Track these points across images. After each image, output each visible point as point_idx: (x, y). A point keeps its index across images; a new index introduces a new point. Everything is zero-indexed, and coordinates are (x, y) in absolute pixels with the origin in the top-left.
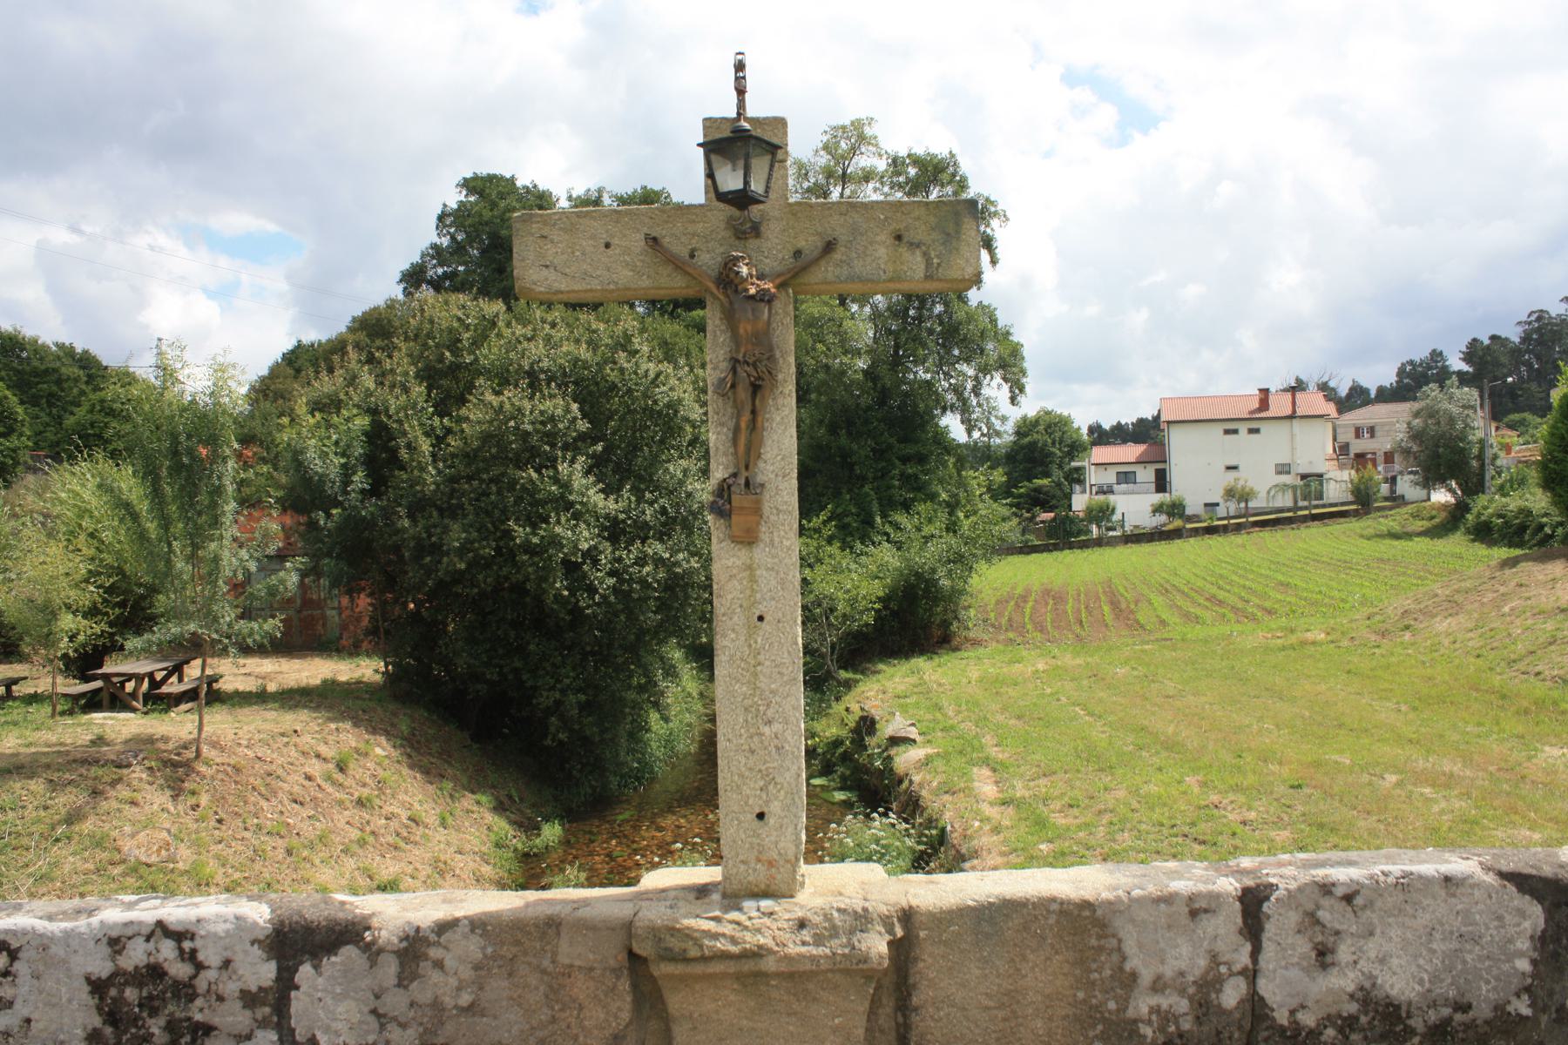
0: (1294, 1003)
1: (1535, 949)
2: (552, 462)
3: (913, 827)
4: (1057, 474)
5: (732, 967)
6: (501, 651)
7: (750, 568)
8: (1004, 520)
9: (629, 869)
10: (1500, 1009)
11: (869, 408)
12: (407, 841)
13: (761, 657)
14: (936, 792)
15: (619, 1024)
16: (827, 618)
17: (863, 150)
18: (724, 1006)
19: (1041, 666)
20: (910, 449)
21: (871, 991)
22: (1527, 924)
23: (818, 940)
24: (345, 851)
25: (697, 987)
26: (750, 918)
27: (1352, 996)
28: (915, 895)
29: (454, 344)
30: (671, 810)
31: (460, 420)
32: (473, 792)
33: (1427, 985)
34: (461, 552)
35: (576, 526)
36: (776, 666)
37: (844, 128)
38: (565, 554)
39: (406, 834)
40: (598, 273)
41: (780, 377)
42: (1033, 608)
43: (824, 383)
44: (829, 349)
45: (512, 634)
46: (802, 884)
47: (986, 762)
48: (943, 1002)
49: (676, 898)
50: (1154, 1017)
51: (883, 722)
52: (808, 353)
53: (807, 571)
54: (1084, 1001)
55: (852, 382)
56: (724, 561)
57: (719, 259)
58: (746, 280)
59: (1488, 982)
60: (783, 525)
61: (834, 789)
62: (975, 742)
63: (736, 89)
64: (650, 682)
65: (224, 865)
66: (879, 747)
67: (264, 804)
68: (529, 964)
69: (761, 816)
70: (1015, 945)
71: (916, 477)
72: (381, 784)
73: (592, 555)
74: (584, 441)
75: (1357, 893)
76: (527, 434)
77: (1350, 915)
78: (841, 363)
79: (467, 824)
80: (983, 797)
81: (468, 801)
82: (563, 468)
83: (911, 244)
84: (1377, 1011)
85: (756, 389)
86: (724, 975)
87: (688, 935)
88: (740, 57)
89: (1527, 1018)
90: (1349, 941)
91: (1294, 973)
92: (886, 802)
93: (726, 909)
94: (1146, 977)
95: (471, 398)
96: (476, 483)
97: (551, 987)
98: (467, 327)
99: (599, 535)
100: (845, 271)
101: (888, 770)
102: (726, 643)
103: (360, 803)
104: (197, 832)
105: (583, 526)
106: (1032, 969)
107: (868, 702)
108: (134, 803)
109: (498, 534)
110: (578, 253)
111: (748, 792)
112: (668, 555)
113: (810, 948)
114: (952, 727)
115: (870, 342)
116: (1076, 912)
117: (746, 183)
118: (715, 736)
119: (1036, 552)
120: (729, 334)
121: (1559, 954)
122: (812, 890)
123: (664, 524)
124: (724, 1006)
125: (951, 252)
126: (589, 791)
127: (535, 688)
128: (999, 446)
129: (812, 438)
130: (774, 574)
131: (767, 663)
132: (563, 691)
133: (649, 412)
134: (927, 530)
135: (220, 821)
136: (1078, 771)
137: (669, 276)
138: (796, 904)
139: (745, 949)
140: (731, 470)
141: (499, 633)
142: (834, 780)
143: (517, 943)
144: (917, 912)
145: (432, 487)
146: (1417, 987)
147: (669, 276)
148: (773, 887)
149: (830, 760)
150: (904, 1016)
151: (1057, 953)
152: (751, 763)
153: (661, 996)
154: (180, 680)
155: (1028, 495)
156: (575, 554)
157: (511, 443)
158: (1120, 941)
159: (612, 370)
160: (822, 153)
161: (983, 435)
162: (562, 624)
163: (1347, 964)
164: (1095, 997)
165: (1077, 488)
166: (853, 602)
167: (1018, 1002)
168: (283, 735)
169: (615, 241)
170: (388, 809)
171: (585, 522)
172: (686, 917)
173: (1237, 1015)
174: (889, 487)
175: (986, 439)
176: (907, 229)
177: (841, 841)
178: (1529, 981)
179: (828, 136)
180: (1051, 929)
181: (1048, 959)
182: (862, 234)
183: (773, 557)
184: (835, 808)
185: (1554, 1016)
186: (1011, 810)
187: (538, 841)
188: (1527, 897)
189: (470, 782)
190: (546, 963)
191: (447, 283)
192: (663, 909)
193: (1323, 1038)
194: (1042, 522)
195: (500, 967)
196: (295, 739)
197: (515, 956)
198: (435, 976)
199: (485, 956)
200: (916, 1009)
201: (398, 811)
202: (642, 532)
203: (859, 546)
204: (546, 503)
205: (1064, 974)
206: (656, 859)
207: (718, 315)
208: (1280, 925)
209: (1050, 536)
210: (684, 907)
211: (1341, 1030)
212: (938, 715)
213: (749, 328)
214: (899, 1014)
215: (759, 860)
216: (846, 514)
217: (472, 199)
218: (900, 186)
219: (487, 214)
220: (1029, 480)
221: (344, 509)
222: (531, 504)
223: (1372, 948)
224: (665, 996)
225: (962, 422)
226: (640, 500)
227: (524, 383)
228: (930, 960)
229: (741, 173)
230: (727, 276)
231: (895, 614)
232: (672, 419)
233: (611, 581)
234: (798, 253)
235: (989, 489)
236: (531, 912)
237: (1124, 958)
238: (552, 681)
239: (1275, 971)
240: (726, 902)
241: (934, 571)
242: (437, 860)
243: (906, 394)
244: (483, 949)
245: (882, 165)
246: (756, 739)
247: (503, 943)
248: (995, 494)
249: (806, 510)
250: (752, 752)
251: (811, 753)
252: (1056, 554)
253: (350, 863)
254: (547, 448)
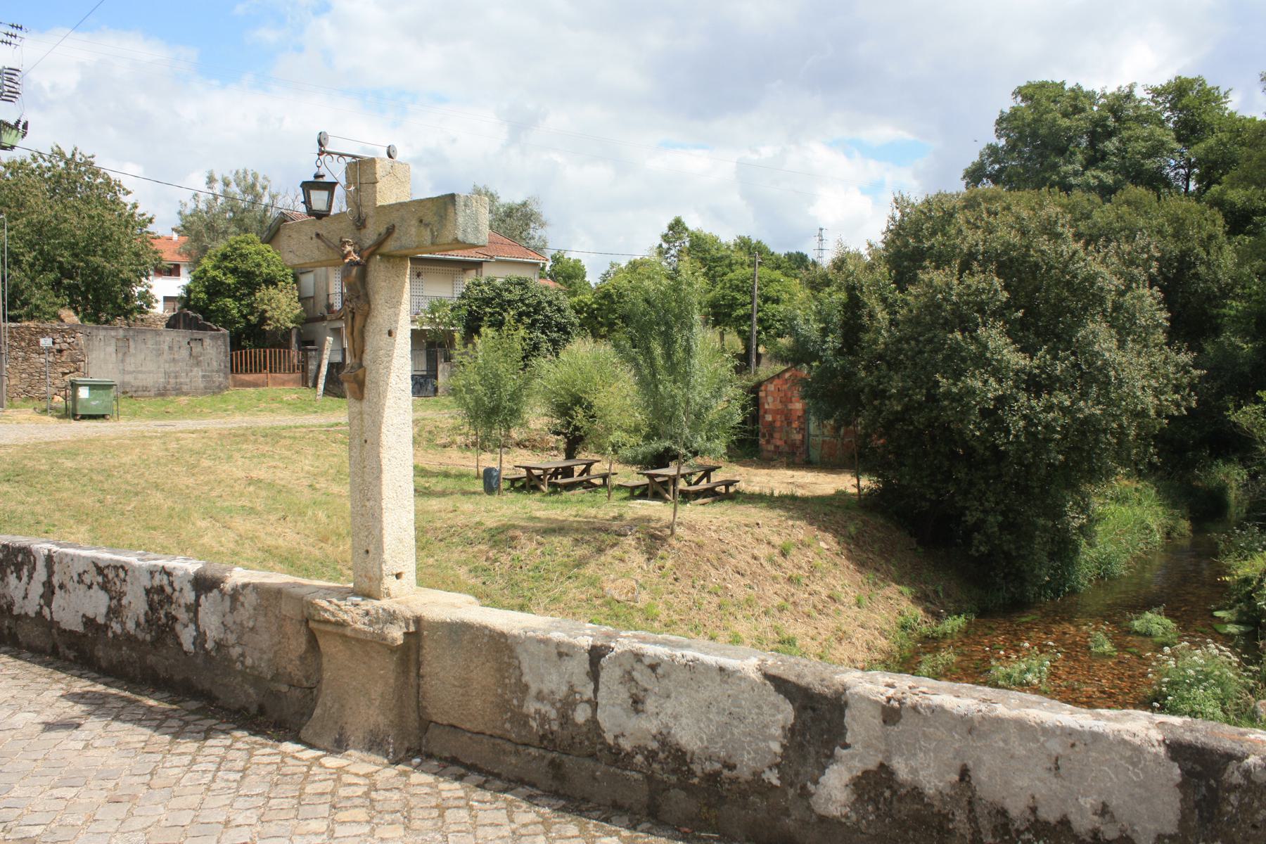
0: (617, 731)
1: (785, 737)
7: (361, 413)
10: (757, 774)
12: (820, 612)
22: (780, 717)
23: (371, 624)
24: (766, 613)
27: (654, 737)
32: (898, 583)
33: (706, 743)
39: (821, 607)
50: (537, 716)
59: (749, 753)
65: (669, 609)
67: (713, 572)
72: (813, 569)
75: (658, 665)
77: (654, 679)
84: (670, 752)
89: (776, 787)
90: (653, 698)
91: (617, 710)
94: (534, 689)
103: (790, 580)
104: (657, 584)
106: (476, 668)
108: (622, 560)
121: (804, 746)
135: (676, 580)
145: (882, 346)
146: (699, 743)
154: (709, 481)
158: (520, 662)
163: (652, 714)
168: (746, 525)
170: (813, 587)
173: (585, 729)
178: (779, 760)
181: (483, 664)
185: (799, 791)
188: (782, 696)
193: (635, 761)
196: (756, 530)
198: (242, 610)
201: (821, 590)
208: (610, 674)
211: (646, 758)
221: (821, 362)
223: (669, 706)
226: (1055, 358)
237: (522, 674)
239: (605, 706)
242: (839, 629)
253: (766, 621)
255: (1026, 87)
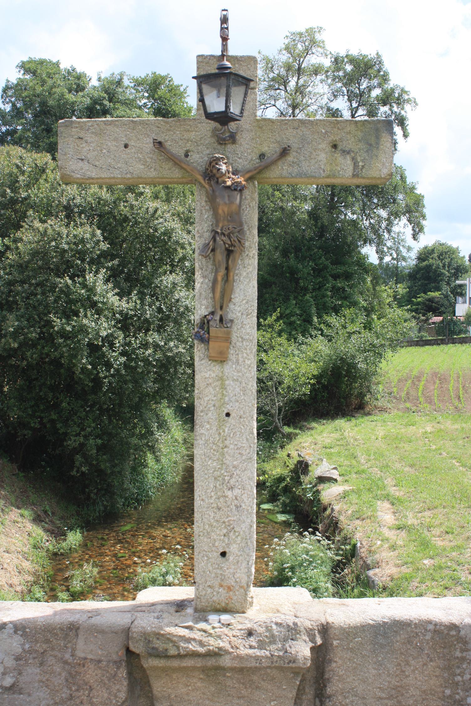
2: (82, 273)
3: (333, 543)
4: (446, 289)
5: (199, 663)
6: (42, 407)
7: (221, 379)
8: (405, 321)
9: (129, 566)
11: (311, 239)
13: (227, 442)
14: (351, 518)
15: (118, 702)
16: (276, 389)
17: (314, 51)
18: (193, 690)
19: (429, 429)
20: (340, 269)
21: (298, 683)
23: (261, 645)
25: (174, 676)
26: (214, 628)
28: (331, 615)
29: (14, 185)
30: (159, 523)
31: (15, 241)
32: (19, 508)
34: (15, 335)
35: (98, 319)
36: (237, 449)
37: (301, 34)
38: (90, 339)
40: (119, 165)
41: (247, 244)
42: (425, 385)
43: (280, 220)
44: (283, 195)
45: (51, 395)
46: (251, 604)
47: (387, 497)
48: (349, 692)
49: (161, 611)
51: (314, 466)
52: (269, 199)
53: (263, 355)
54: (450, 697)
55: (300, 220)
56: (203, 374)
57: (206, 159)
58: (225, 175)
60: (246, 349)
61: (278, 513)
62: (380, 483)
63: (221, 37)
64: (148, 431)
66: (311, 483)
68: (55, 657)
69: (223, 554)
70: (401, 653)
71: (343, 289)
73: (109, 340)
74: (105, 258)
76: (64, 251)
78: (292, 206)
79: (13, 531)
80: (384, 523)
81: (14, 514)
82: (90, 277)
83: (344, 151)
85: (229, 252)
86: (194, 668)
87: (169, 639)
88: (225, 13)
92: (315, 523)
93: (197, 621)
95: (24, 224)
96: (26, 286)
97: (70, 674)
98: (23, 173)
99: (115, 326)
100: (295, 170)
101: (316, 500)
102: (202, 431)
105: (104, 319)
106: (413, 671)
107: (304, 450)
109: (42, 323)
110: (104, 151)
111: (215, 537)
112: (163, 344)
113: (256, 650)
114: (363, 471)
115: (314, 191)
116: (446, 632)
117: (227, 107)
118: (193, 471)
119: (430, 345)
120: (211, 213)
122: (258, 608)
123: (161, 319)
124: (193, 690)
125: (372, 158)
126: (102, 508)
127: (66, 434)
128: (404, 268)
129: (269, 259)
130: (238, 383)
131: (232, 446)
132: (85, 437)
133: (151, 238)
134: (351, 328)
136: (453, 507)
137: (170, 169)
138: (246, 618)
139: (209, 650)
140: (210, 310)
141: (41, 394)
142: (277, 506)
143: (47, 641)
144: (331, 627)
147: (170, 169)
148: (231, 605)
149: (275, 491)
150: (321, 701)
151: (431, 660)
152: (218, 517)
153: (149, 681)
155: (424, 303)
156: (97, 339)
157: (52, 258)
159: (125, 207)
160: (284, 52)
161: (393, 259)
162: (86, 389)
164: (458, 694)
165: (460, 299)
166: (295, 378)
167: (402, 695)
169: (131, 143)
171: (105, 316)
172: (170, 624)
174: (324, 296)
175: (395, 262)
176: (341, 140)
177: (281, 553)
179: (289, 40)
180: (428, 643)
181: (425, 664)
182: (308, 143)
183: (238, 372)
184: (277, 526)
186: (403, 534)
187: (64, 544)
189: (16, 500)
190: (67, 656)
191: (9, 138)
192: (152, 619)
194: (434, 323)
195: (34, 658)
197: (45, 651)
199: (24, 650)
200: (329, 697)
202: (145, 326)
203: (300, 338)
204: (77, 302)
205: (436, 676)
206: (149, 561)
207: (204, 198)
209: (438, 334)
210: (167, 617)
212: (354, 462)
213: (226, 210)
214: (317, 700)
215: (221, 586)
216: (291, 314)
217: (28, 77)
218: (340, 80)
219: (39, 89)
220: (425, 293)
222: (66, 303)
224: (151, 682)
225: (377, 252)
227: (62, 215)
228: (340, 662)
229: (223, 99)
230: (211, 171)
231: (325, 387)
232: (166, 243)
233: (123, 359)
234: (262, 156)
235: (395, 297)
236: (58, 619)
238: (78, 430)
240: (197, 615)
241: (353, 357)
243: (339, 230)
244: (23, 645)
245: (327, 63)
246: (222, 500)
247: (37, 641)
248: (400, 302)
249: (262, 312)
250: (219, 509)
251: (260, 485)
252: (442, 347)
254: (79, 262)
255: (29, 62)
